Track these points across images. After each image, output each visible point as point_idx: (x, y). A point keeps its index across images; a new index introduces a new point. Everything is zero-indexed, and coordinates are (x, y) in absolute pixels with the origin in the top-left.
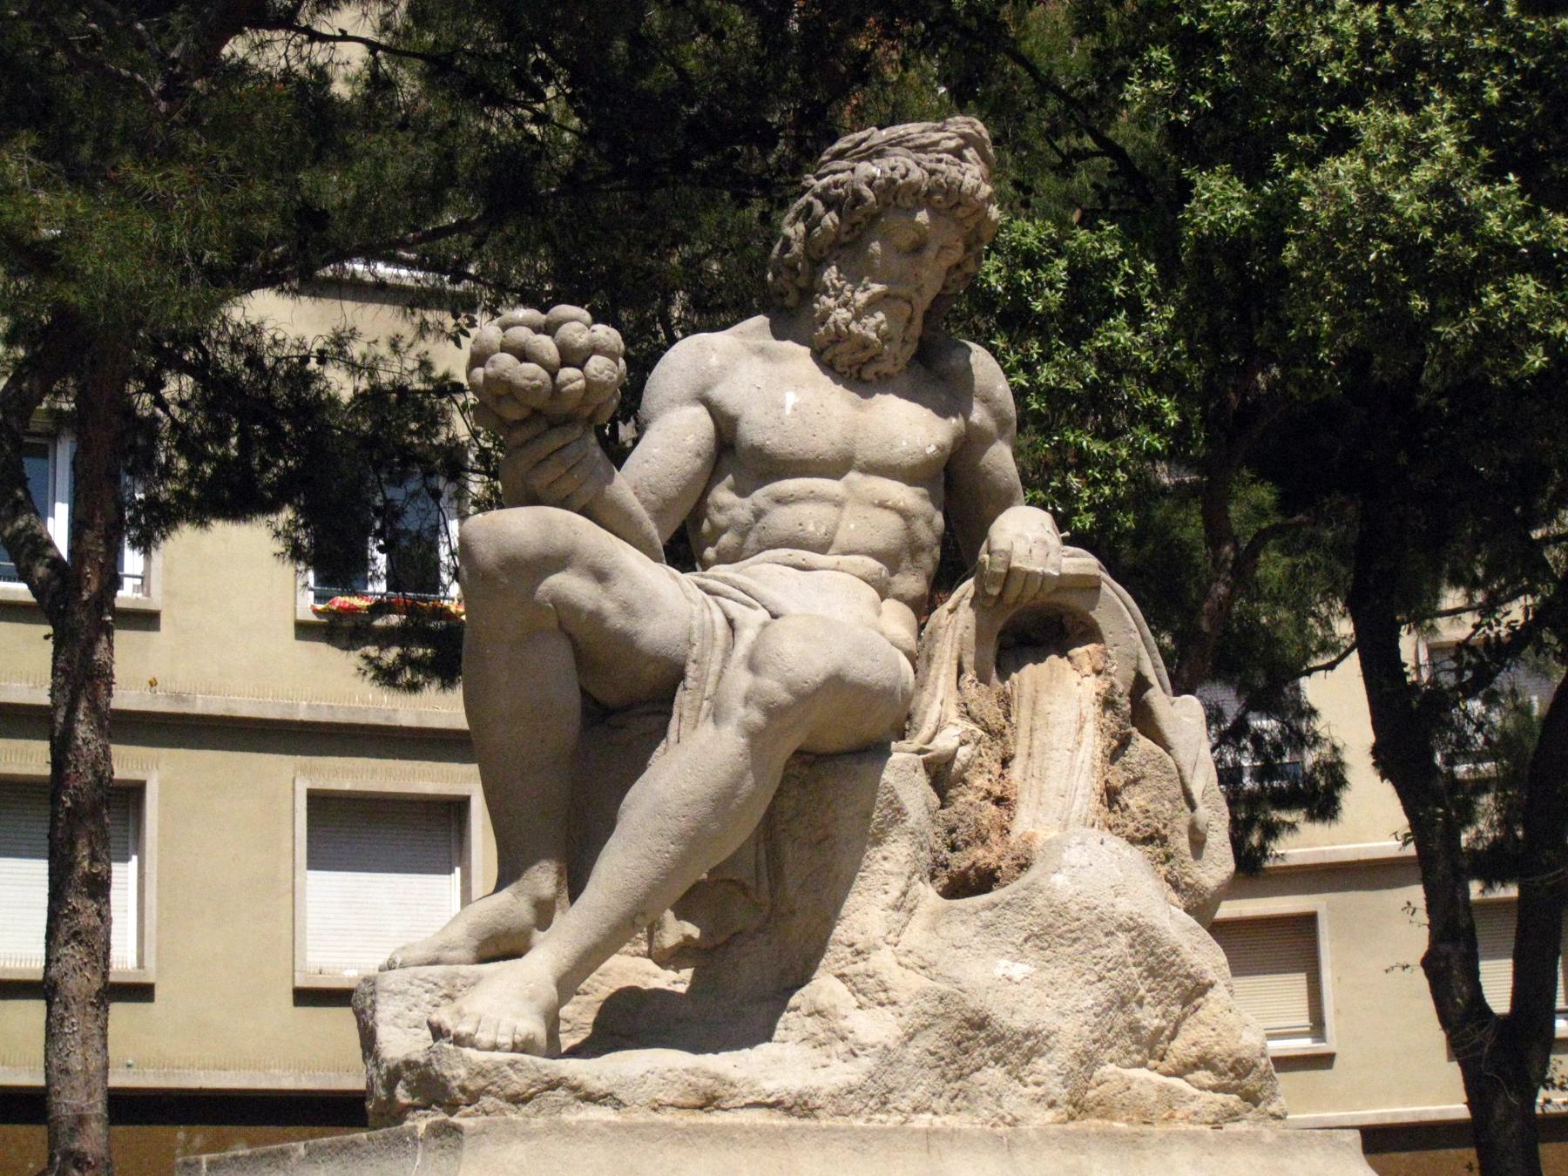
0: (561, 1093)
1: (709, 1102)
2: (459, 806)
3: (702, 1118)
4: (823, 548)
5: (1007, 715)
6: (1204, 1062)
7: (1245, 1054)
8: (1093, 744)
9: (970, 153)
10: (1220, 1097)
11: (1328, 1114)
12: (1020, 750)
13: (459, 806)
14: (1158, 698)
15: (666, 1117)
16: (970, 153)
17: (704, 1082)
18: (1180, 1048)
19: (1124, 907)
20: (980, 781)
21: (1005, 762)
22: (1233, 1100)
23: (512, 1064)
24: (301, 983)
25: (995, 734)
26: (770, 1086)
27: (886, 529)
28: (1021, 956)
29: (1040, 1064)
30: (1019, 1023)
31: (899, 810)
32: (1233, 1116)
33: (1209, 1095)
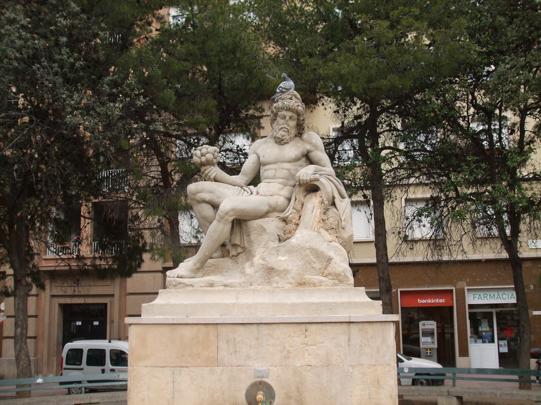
0: (182, 285)
1: (212, 285)
2: (452, 290)
3: (211, 288)
4: (273, 178)
5: (302, 208)
6: (330, 274)
7: (338, 272)
8: (318, 212)
9: (293, 98)
10: (333, 281)
11: (437, 301)
12: (302, 214)
13: (452, 290)
14: (338, 200)
15: (202, 288)
16: (293, 98)
17: (211, 282)
18: (326, 272)
19: (308, 245)
20: (294, 221)
21: (300, 217)
22: (336, 281)
23: (174, 280)
24: (82, 371)
25: (298, 211)
26: (225, 282)
27: (284, 173)
28: (285, 256)
29: (288, 276)
30: (281, 269)
31: (306, 229)
32: (336, 285)
33: (331, 280)
